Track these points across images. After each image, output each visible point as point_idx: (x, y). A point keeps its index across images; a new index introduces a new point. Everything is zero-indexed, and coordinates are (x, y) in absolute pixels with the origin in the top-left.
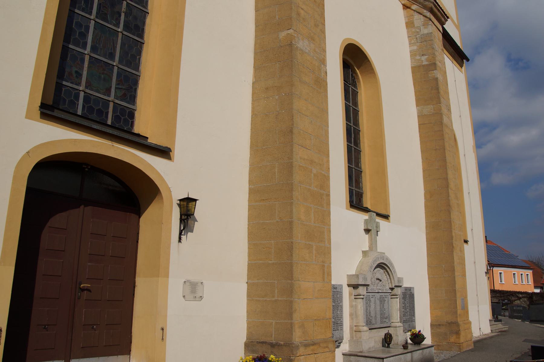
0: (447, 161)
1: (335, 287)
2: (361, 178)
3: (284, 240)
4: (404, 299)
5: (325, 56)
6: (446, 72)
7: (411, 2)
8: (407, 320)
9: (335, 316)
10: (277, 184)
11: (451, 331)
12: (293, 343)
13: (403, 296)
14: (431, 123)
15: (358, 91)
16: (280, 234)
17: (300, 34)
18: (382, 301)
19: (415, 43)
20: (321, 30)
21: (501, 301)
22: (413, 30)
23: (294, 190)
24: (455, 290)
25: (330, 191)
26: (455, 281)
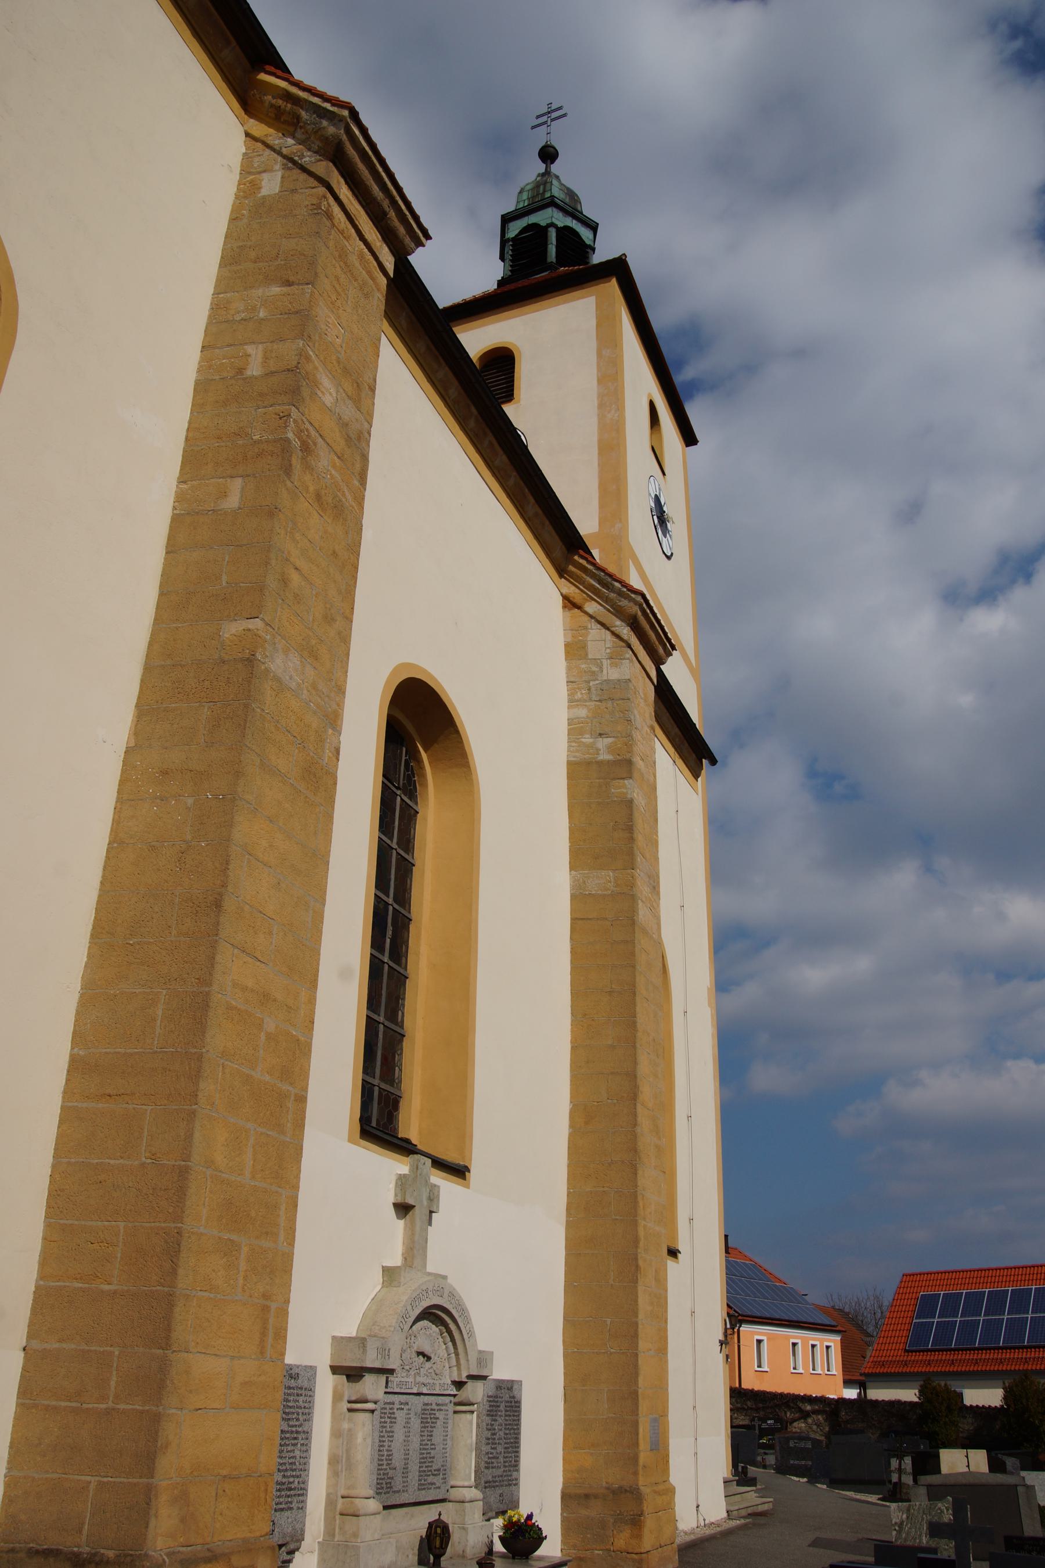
0: (638, 1025)
1: (292, 1374)
2: (399, 1052)
3: (158, 1224)
4: (492, 1416)
5: (340, 705)
6: (656, 788)
7: (585, 593)
8: (497, 1479)
9: (285, 1464)
10: (156, 1052)
11: (618, 1515)
12: (146, 1555)
13: (490, 1406)
14: (606, 919)
15: (419, 808)
16: (147, 1205)
17: (280, 635)
18: (428, 1419)
19: (586, 701)
20: (339, 633)
21: (757, 1423)
22: (583, 666)
23: (206, 1075)
24: (636, 1393)
25: (307, 1088)
26: (636, 1366)
